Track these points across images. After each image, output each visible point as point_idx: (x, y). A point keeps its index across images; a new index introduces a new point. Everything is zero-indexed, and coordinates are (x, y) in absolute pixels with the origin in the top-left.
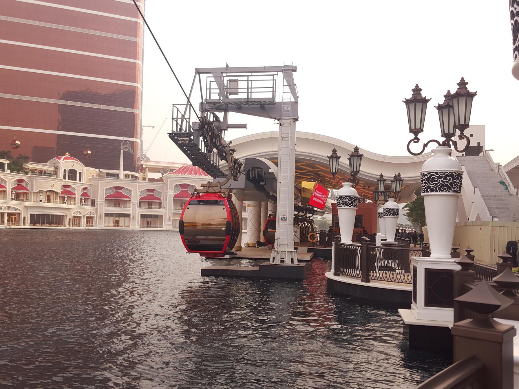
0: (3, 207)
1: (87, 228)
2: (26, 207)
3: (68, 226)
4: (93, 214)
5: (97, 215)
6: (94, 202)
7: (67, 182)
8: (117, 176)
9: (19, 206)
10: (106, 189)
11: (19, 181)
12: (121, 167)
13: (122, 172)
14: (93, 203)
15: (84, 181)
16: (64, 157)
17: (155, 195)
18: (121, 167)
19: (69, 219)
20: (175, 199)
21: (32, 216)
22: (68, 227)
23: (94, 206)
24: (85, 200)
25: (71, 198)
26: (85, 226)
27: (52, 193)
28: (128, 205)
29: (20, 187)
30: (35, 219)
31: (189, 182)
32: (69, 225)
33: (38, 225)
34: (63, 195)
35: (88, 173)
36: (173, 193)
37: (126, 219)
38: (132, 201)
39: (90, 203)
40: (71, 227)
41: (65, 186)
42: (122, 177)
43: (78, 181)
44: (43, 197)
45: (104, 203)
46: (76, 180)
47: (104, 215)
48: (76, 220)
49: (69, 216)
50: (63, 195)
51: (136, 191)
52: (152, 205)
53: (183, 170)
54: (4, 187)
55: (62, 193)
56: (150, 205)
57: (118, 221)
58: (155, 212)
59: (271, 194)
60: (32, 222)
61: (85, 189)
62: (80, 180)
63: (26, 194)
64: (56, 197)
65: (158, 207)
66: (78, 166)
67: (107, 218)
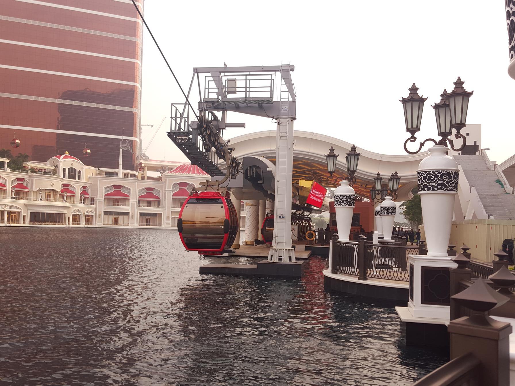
0: (3, 206)
1: (86, 226)
2: (26, 205)
3: (67, 224)
4: (92, 212)
5: (96, 213)
6: (94, 200)
7: (67, 180)
8: (116, 174)
9: (19, 204)
10: (105, 188)
11: (19, 179)
12: (121, 166)
13: (121, 171)
14: (93, 201)
15: (83, 180)
16: (63, 156)
17: (154, 193)
18: (121, 166)
19: (69, 218)
20: (174, 197)
21: (32, 214)
22: (67, 225)
23: (94, 204)
24: (85, 198)
25: (70, 196)
26: (84, 224)
27: (52, 191)
28: (127, 204)
29: (20, 186)
30: (35, 217)
31: (187, 180)
32: (69, 224)
33: (38, 223)
34: (63, 194)
35: (87, 172)
36: (171, 192)
37: (126, 217)
38: (131, 200)
39: (89, 202)
40: (71, 226)
41: (64, 185)
42: (121, 175)
43: (77, 180)
44: (43, 196)
45: (103, 201)
46: (75, 179)
47: (103, 214)
48: (76, 218)
49: (69, 214)
50: (63, 194)
51: (135, 189)
52: (150, 204)
53: (182, 169)
54: (4, 186)
55: (62, 191)
56: (149, 204)
57: (118, 219)
58: (154, 210)
59: (269, 193)
60: (31, 221)
61: (84, 187)
62: (79, 179)
63: (26, 192)
64: (56, 195)
65: (157, 205)
66: (77, 165)
67: (106, 216)
